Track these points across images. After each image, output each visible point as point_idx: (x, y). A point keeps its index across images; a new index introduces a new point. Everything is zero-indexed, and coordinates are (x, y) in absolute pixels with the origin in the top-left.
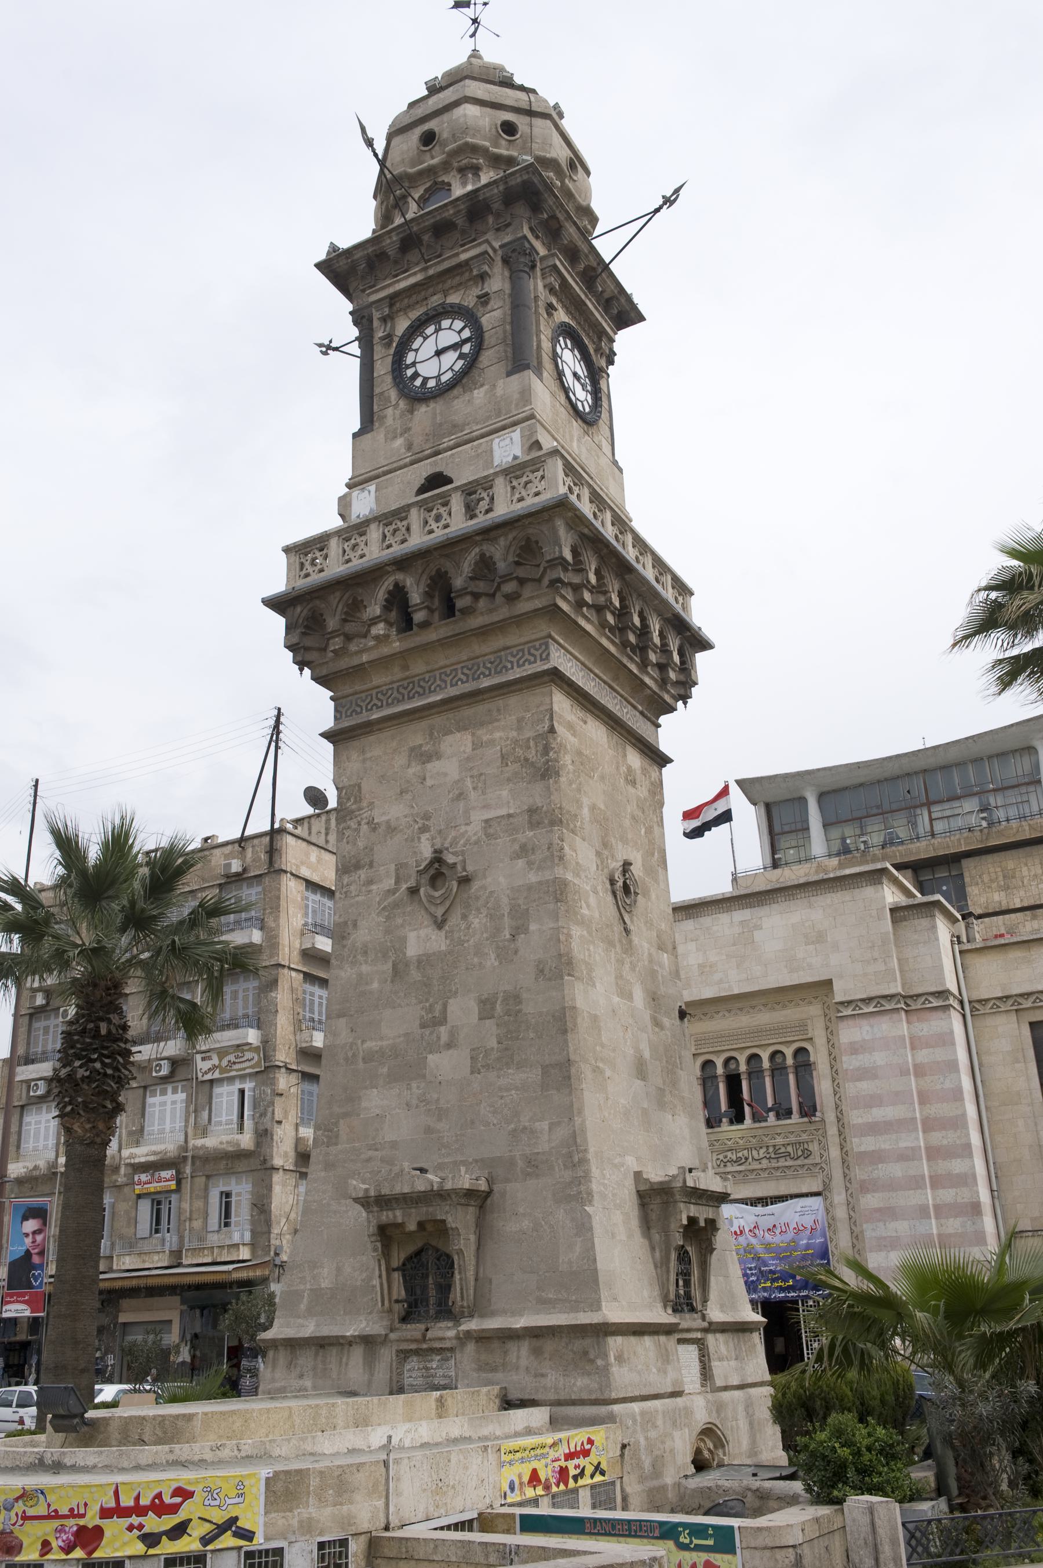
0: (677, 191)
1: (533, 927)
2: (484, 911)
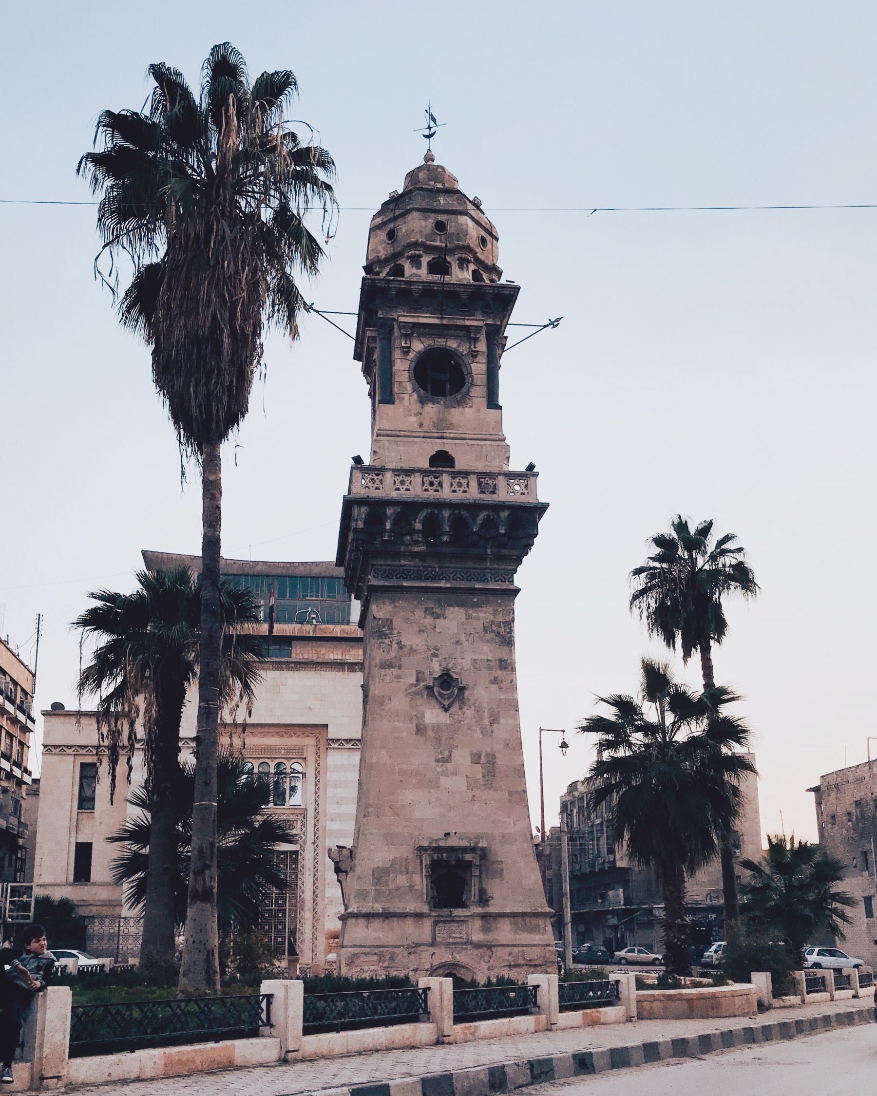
0: (558, 320)
1: (502, 721)
2: (473, 708)
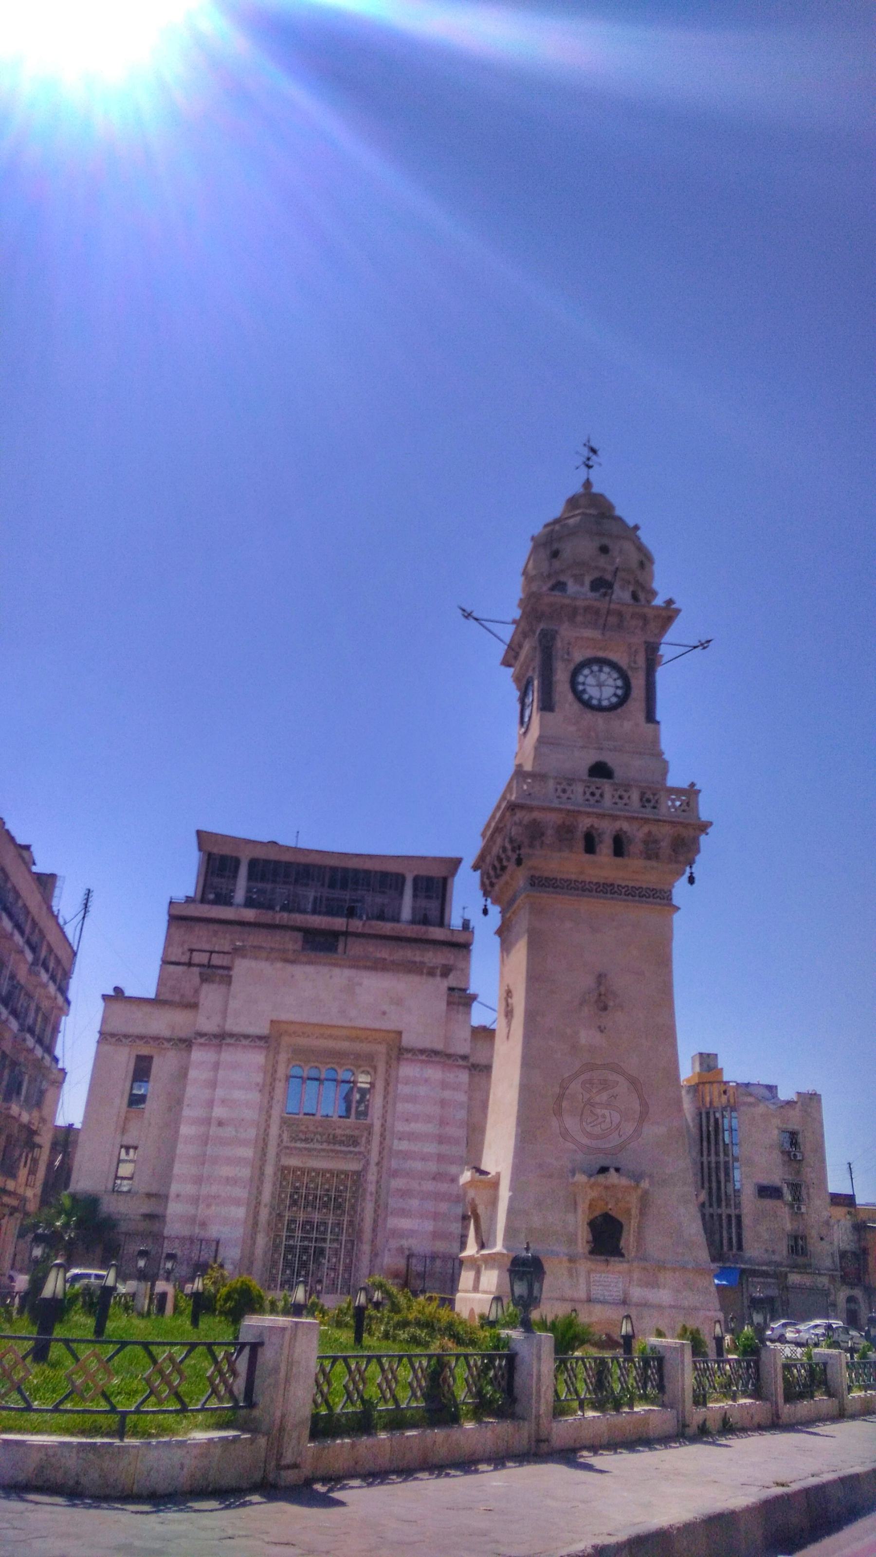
0: (709, 641)
